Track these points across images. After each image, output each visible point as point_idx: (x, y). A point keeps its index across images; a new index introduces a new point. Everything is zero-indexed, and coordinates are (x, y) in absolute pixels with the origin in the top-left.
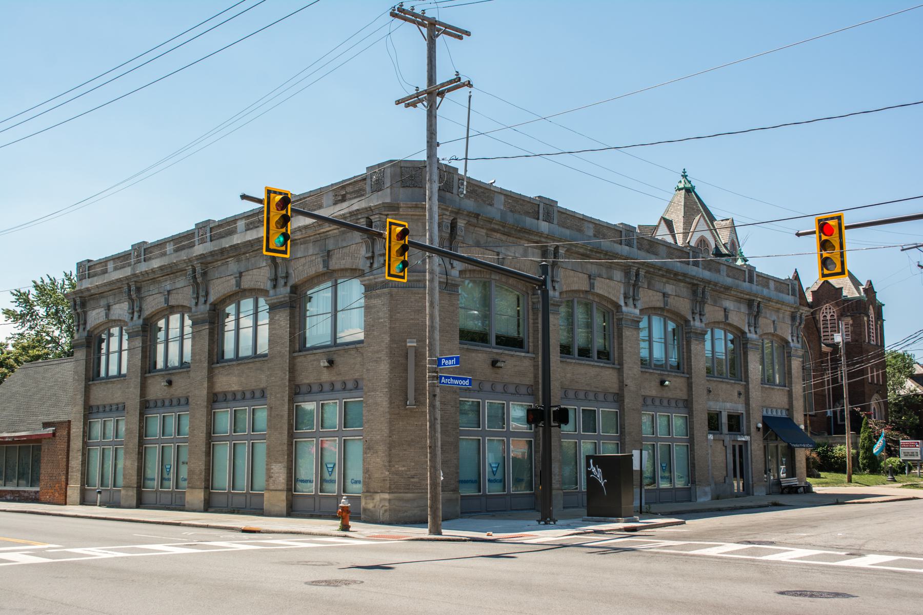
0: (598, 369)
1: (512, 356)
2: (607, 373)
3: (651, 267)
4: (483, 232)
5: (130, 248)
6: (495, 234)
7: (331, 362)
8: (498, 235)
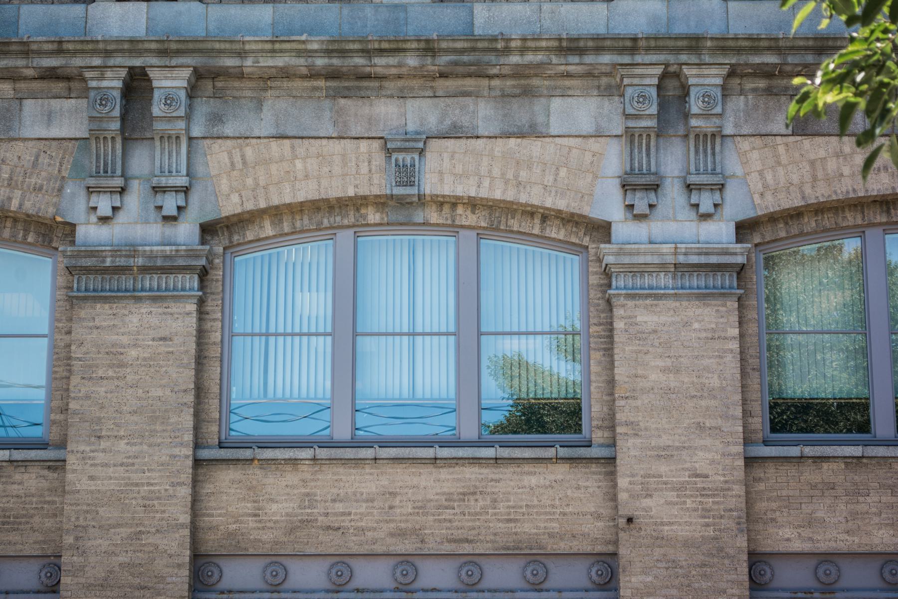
0: (471, 473)
2: (534, 480)
3: (756, 50)
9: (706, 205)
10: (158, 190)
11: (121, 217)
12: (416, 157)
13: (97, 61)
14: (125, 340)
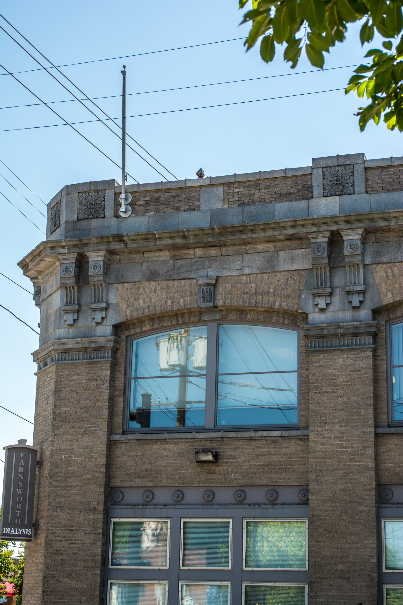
1: (251, 439)
4: (165, 255)
5: (310, 164)
6: (192, 251)
7: (216, 456)
8: (199, 252)
9: (356, 303)
10: (349, 293)
11: (331, 308)
12: (212, 287)
13: (314, 229)
14: (336, 372)
